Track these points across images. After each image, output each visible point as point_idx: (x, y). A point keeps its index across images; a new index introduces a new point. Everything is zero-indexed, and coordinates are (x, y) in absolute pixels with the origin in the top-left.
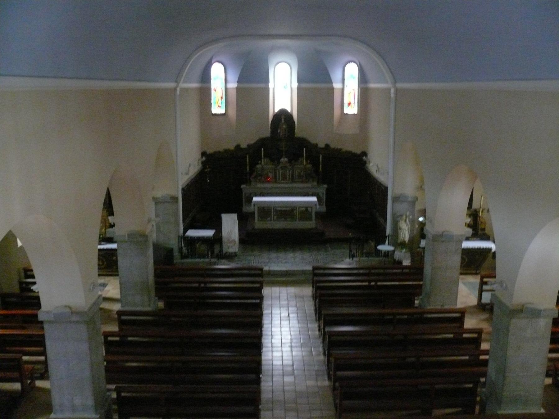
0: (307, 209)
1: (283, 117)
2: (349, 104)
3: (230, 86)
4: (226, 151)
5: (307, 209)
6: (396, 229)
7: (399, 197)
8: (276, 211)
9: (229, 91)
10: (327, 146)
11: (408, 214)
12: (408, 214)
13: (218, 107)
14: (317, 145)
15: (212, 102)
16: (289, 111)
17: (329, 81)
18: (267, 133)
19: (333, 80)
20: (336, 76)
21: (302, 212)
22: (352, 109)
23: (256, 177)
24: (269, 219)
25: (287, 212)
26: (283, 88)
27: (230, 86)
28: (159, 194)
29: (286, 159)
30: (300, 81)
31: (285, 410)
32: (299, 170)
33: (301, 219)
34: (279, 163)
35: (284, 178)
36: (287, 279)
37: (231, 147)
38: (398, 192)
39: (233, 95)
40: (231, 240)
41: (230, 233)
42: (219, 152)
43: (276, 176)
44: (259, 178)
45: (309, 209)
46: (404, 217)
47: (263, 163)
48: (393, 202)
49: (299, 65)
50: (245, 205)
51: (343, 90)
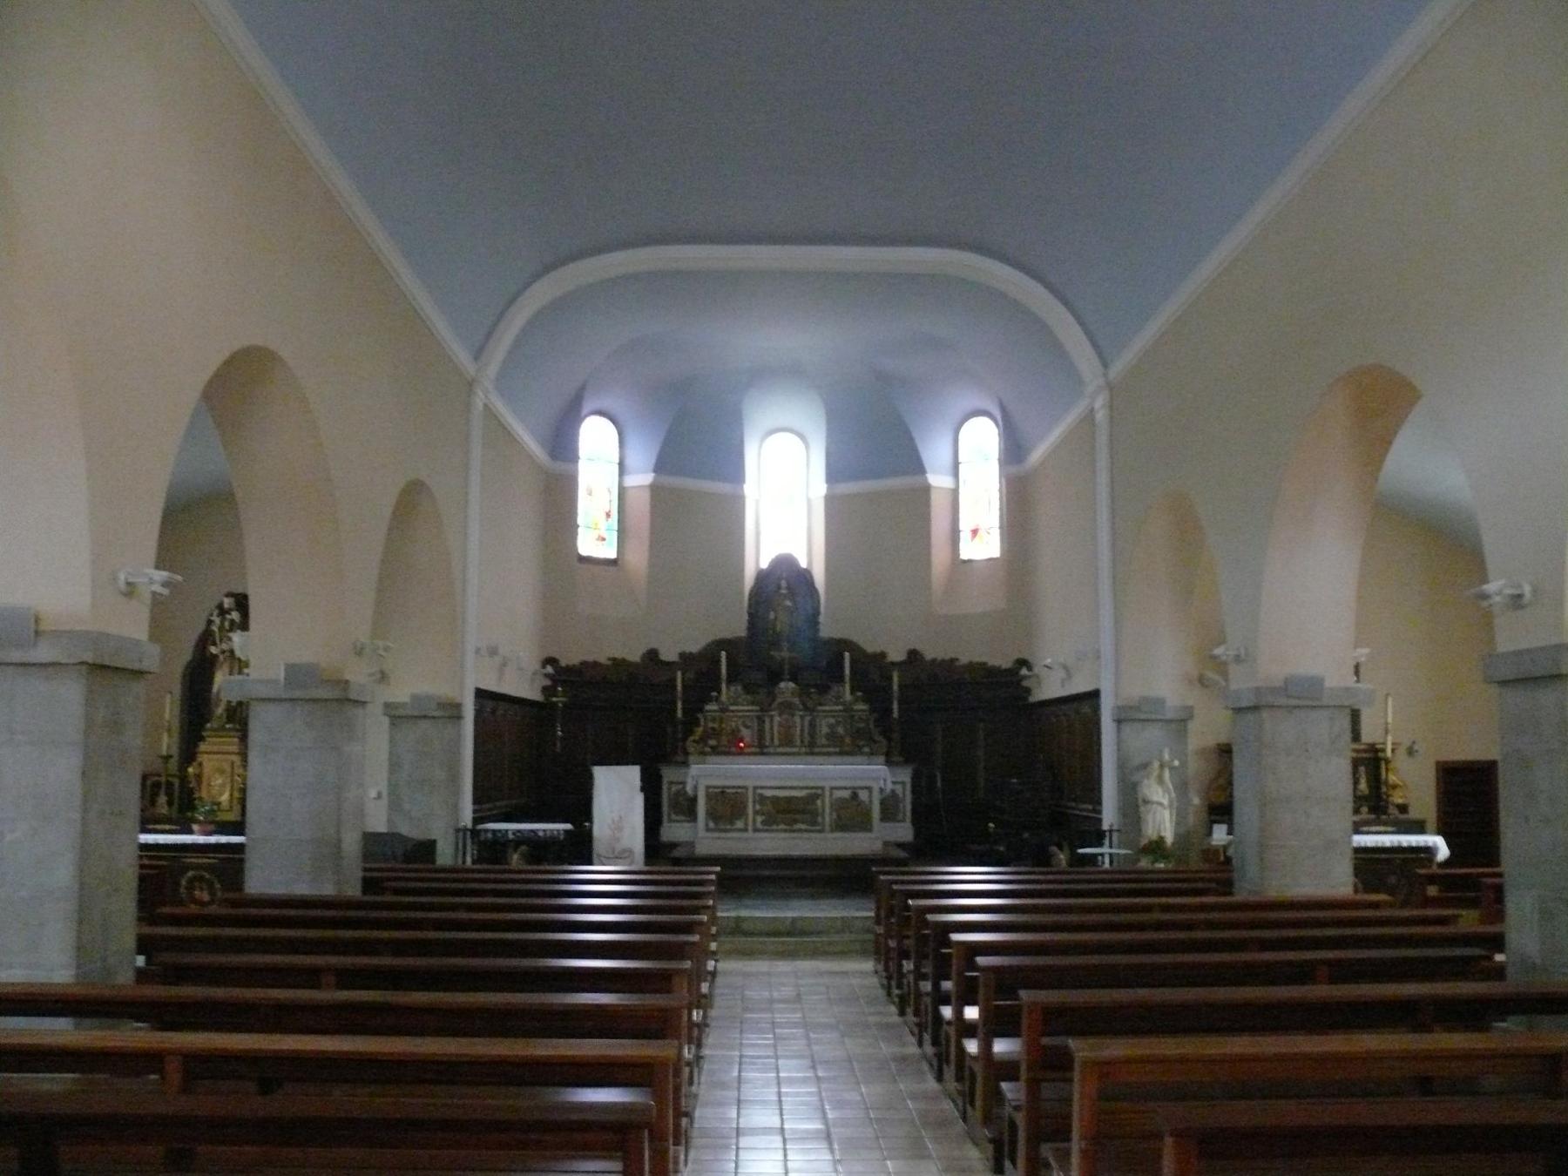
0: (855, 796)
1: (785, 580)
2: (975, 532)
3: (630, 481)
4: (618, 663)
5: (855, 796)
6: (1132, 806)
7: (1138, 709)
8: (762, 799)
9: (631, 497)
10: (914, 655)
11: (1166, 757)
12: (1166, 757)
13: (596, 535)
14: (883, 655)
15: (580, 521)
16: (803, 564)
17: (917, 467)
18: (737, 627)
19: (927, 466)
20: (935, 454)
21: (840, 805)
22: (982, 541)
23: (703, 740)
24: (739, 824)
25: (790, 811)
26: (784, 501)
27: (630, 481)
28: (401, 693)
29: (792, 685)
30: (832, 476)
31: (782, 1129)
32: (832, 721)
33: (841, 826)
34: (772, 696)
35: (787, 740)
36: (790, 374)
37: (635, 655)
38: (1134, 691)
39: (641, 506)
40: (619, 847)
41: (618, 827)
42: (596, 664)
43: (761, 737)
44: (712, 742)
45: (863, 795)
46: (1156, 764)
47: (724, 698)
48: (1119, 722)
49: (829, 422)
50: (670, 821)
51: (955, 492)
